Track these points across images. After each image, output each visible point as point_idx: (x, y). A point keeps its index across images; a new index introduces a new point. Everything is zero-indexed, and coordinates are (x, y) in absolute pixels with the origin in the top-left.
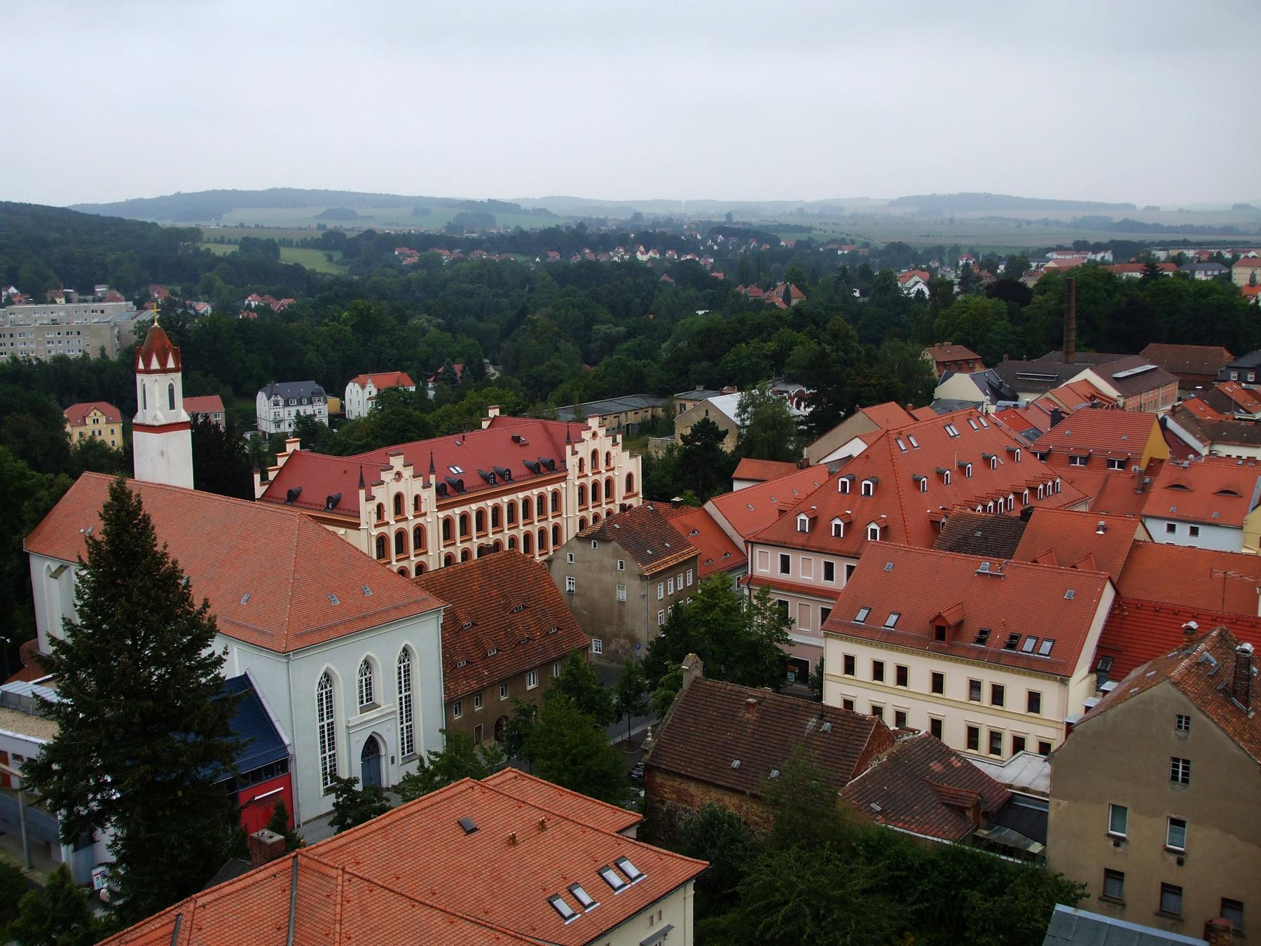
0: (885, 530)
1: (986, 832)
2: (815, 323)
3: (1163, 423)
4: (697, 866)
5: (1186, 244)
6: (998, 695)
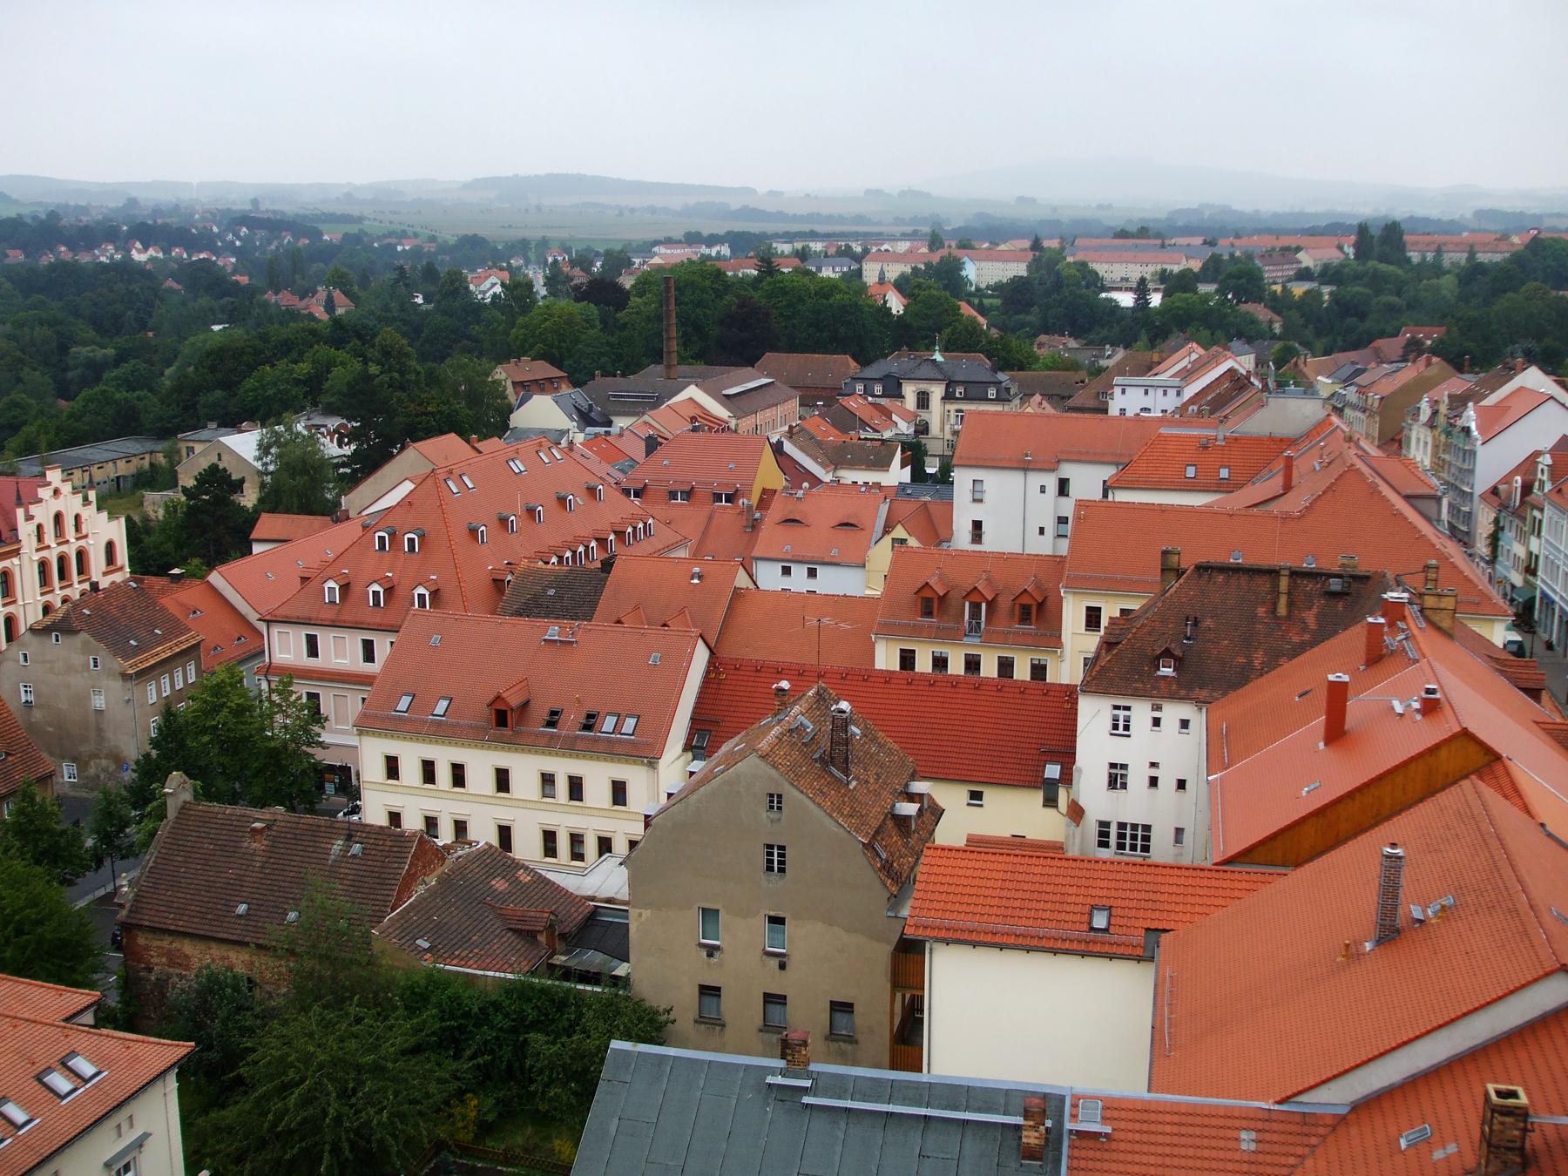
0: (435, 594)
1: (563, 958)
2: (359, 336)
3: (778, 449)
4: (180, 1049)
5: (814, 235)
6: (576, 788)
